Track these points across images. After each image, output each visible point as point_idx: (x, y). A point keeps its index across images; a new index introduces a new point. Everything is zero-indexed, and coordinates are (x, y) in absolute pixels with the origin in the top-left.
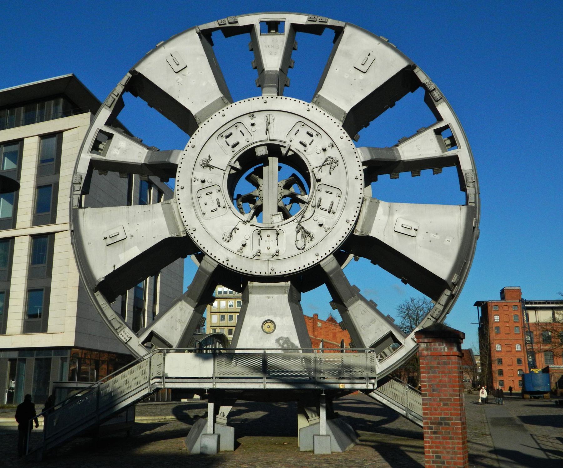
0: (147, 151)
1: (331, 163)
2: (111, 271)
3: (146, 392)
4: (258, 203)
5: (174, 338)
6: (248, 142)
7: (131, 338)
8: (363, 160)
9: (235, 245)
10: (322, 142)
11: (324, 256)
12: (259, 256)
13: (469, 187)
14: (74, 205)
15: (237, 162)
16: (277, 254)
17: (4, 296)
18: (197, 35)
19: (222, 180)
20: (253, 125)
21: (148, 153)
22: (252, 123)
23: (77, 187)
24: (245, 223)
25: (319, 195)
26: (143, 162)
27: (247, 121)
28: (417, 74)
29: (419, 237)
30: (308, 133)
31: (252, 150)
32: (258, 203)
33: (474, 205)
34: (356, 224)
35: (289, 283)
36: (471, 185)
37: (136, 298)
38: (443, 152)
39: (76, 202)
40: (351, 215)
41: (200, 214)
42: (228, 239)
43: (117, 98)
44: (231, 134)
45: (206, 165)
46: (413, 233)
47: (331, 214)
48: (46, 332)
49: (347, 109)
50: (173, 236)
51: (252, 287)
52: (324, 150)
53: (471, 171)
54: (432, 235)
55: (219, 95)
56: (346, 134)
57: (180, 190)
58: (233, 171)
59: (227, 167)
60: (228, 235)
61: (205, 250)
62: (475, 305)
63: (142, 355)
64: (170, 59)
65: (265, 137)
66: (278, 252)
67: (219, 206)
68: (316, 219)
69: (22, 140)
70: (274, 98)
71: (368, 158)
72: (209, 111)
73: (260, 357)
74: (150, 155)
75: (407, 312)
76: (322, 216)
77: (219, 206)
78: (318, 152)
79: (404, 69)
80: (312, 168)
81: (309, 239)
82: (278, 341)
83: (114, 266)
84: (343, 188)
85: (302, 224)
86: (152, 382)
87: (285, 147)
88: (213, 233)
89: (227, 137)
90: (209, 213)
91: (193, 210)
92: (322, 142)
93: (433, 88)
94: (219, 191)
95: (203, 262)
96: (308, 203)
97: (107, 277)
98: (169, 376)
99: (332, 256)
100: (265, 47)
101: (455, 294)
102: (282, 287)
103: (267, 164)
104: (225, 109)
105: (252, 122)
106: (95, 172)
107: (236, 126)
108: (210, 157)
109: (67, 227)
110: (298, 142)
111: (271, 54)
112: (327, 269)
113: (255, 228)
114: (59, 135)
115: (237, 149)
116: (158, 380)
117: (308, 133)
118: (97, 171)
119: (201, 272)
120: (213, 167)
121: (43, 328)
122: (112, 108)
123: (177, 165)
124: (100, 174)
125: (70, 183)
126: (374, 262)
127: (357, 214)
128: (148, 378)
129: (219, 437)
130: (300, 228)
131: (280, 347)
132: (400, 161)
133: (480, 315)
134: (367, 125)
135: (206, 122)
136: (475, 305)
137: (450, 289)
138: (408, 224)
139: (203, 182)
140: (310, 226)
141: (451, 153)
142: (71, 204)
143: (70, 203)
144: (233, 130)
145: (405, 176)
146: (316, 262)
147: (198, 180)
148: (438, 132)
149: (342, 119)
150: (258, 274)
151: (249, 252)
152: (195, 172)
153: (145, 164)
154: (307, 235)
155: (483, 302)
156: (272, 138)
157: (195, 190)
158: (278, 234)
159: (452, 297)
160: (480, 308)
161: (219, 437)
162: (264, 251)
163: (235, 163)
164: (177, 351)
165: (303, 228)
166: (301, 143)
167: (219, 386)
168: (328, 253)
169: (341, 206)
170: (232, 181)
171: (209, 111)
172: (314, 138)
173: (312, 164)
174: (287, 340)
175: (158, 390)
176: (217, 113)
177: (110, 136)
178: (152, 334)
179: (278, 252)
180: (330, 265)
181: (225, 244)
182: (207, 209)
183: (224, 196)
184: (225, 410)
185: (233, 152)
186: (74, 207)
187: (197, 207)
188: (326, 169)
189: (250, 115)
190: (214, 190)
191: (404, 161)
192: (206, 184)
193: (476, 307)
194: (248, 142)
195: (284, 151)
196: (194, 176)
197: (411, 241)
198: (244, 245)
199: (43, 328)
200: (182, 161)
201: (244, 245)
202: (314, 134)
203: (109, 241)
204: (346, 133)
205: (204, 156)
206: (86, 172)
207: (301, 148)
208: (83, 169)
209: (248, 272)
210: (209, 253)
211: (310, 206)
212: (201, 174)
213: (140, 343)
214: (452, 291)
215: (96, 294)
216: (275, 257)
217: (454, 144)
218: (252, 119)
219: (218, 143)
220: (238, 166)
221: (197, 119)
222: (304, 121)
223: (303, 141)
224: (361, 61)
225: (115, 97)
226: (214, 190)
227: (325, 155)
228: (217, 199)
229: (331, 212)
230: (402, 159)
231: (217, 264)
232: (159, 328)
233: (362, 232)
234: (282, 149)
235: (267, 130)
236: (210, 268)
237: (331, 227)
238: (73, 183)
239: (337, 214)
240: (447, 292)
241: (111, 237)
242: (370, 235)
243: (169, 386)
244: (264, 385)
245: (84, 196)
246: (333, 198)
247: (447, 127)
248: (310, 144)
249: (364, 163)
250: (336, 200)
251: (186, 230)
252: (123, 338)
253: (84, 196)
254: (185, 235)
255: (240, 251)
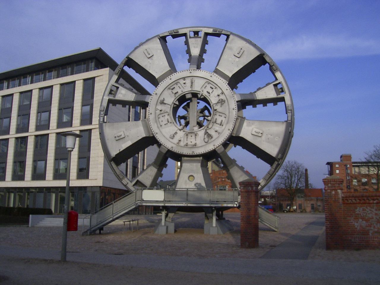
0: (135, 95)
1: (221, 102)
2: (118, 152)
3: (134, 207)
4: (188, 120)
5: (148, 183)
6: (182, 91)
7: (128, 183)
8: (237, 100)
9: (176, 140)
10: (218, 92)
11: (217, 146)
12: (187, 145)
13: (289, 112)
14: (101, 121)
15: (177, 101)
16: (195, 145)
17: (27, 116)
18: (159, 40)
19: (169, 109)
20: (184, 83)
21: (135, 96)
22: (184, 82)
23: (102, 113)
24: (180, 130)
25: (216, 117)
26: (133, 100)
27: (182, 82)
28: (265, 58)
29: (264, 137)
30: (211, 87)
31: (184, 96)
32: (188, 120)
33: (290, 121)
34: (233, 130)
35: (201, 158)
36: (290, 111)
37: (133, 162)
38: (277, 95)
39: (102, 120)
40: (231, 126)
41: (159, 126)
42: (172, 138)
43: (120, 70)
44: (174, 88)
45: (162, 103)
46: (260, 135)
47: (221, 126)
48: (88, 178)
49: (230, 76)
50: (147, 136)
51: (184, 160)
52: (218, 95)
53: (291, 105)
54: (269, 136)
55: (169, 69)
56: (229, 88)
57: (150, 115)
58: (175, 106)
59: (172, 104)
60: (172, 136)
61: (162, 143)
62: (327, 164)
63: (133, 190)
64: (146, 52)
65: (190, 89)
66: (196, 144)
67: (168, 122)
68: (214, 128)
69: (75, 82)
70: (195, 70)
71: (239, 99)
72: (164, 76)
73: (185, 192)
74: (136, 97)
75: (286, 168)
76: (217, 127)
77: (168, 122)
78: (216, 96)
79: (258, 56)
80: (212, 104)
81: (210, 137)
82: (195, 185)
83: (120, 150)
84: (227, 113)
85: (208, 131)
86: (136, 202)
87: (200, 94)
88: (165, 135)
89: (172, 89)
90: (163, 126)
91: (156, 124)
92: (218, 92)
93: (273, 65)
94: (168, 115)
95: (161, 148)
96: (211, 121)
97: (116, 155)
98: (144, 200)
99: (221, 146)
100: (192, 44)
101: (280, 163)
102: (197, 160)
103: (191, 101)
104: (171, 76)
105: (184, 82)
106: (111, 105)
107: (177, 84)
108: (164, 99)
109: (98, 126)
110: (206, 91)
111: (195, 47)
112: (219, 152)
113: (185, 133)
114: (93, 79)
115: (177, 95)
116: (139, 202)
117: (211, 87)
118: (112, 104)
119: (160, 153)
120: (165, 104)
121: (87, 177)
122: (118, 74)
123: (148, 103)
124: (113, 105)
125: (99, 111)
126: (243, 148)
127: (233, 126)
128: (135, 201)
129: (167, 227)
130: (206, 133)
131: (196, 188)
132: (256, 100)
133: (329, 170)
134: (241, 81)
135: (162, 82)
136: (327, 164)
137: (277, 161)
138: (258, 130)
139: (161, 111)
140: (211, 132)
141: (282, 95)
142: (99, 120)
143: (99, 120)
144: (175, 86)
145: (260, 107)
146: (213, 148)
147: (158, 110)
148: (275, 86)
149: (228, 80)
150: (186, 154)
151: (182, 144)
152: (157, 106)
153: (134, 101)
154: (209, 136)
155: (331, 163)
156: (193, 90)
157: (157, 114)
158: (196, 135)
159: (278, 165)
160: (329, 166)
161: (167, 227)
162: (189, 143)
163: (176, 101)
164: (149, 189)
165: (208, 133)
166: (207, 92)
167: (166, 205)
168: (219, 144)
169: (226, 122)
170: (175, 109)
171: (164, 76)
172: (214, 89)
173: (212, 102)
174: (200, 184)
175: (139, 206)
176: (167, 78)
177: (118, 88)
178: (138, 181)
179: (196, 144)
180: (220, 150)
181: (171, 140)
182: (163, 124)
183: (171, 118)
184: (171, 215)
185: (175, 96)
186: (101, 122)
187: (158, 122)
188: (219, 105)
189: (183, 78)
190: (166, 114)
191: (258, 100)
192: (162, 112)
193: (327, 165)
194: (182, 91)
195: (199, 96)
196: (157, 108)
197: (260, 138)
198: (180, 141)
199: (87, 177)
200: (151, 101)
201: (180, 141)
202: (214, 87)
203: (117, 138)
204: (229, 87)
205: (161, 98)
206: (106, 105)
207: (207, 94)
208: (105, 104)
209: (182, 153)
210: (163, 144)
211: (211, 122)
212: (160, 107)
213: (132, 185)
214: (278, 162)
215: (111, 163)
216: (194, 146)
217: (282, 91)
218: (184, 81)
219: (167, 93)
220: (177, 103)
221: (158, 80)
222: (209, 82)
223: (209, 91)
224: (237, 52)
225: (119, 69)
226: (166, 114)
227: (219, 98)
228: (168, 119)
229: (221, 125)
230: (258, 99)
231: (167, 149)
232: (140, 178)
233: (236, 134)
234: (198, 95)
235: (191, 86)
236: (164, 151)
237: (221, 132)
238: (100, 111)
239: (224, 126)
240: (276, 163)
241: (118, 137)
242: (240, 136)
243: (144, 204)
244: (187, 205)
245: (105, 116)
246: (222, 118)
247: (279, 83)
248: (212, 93)
249: (237, 102)
250: (224, 119)
251: (153, 133)
252: (124, 183)
253: (105, 116)
254: (152, 135)
255: (178, 143)
